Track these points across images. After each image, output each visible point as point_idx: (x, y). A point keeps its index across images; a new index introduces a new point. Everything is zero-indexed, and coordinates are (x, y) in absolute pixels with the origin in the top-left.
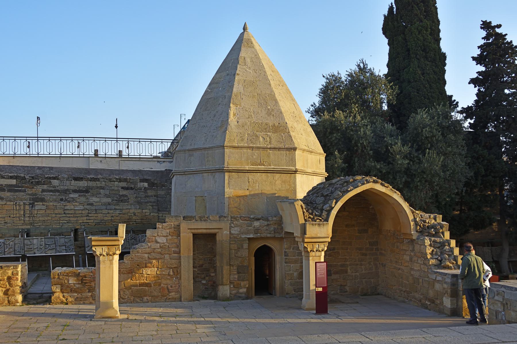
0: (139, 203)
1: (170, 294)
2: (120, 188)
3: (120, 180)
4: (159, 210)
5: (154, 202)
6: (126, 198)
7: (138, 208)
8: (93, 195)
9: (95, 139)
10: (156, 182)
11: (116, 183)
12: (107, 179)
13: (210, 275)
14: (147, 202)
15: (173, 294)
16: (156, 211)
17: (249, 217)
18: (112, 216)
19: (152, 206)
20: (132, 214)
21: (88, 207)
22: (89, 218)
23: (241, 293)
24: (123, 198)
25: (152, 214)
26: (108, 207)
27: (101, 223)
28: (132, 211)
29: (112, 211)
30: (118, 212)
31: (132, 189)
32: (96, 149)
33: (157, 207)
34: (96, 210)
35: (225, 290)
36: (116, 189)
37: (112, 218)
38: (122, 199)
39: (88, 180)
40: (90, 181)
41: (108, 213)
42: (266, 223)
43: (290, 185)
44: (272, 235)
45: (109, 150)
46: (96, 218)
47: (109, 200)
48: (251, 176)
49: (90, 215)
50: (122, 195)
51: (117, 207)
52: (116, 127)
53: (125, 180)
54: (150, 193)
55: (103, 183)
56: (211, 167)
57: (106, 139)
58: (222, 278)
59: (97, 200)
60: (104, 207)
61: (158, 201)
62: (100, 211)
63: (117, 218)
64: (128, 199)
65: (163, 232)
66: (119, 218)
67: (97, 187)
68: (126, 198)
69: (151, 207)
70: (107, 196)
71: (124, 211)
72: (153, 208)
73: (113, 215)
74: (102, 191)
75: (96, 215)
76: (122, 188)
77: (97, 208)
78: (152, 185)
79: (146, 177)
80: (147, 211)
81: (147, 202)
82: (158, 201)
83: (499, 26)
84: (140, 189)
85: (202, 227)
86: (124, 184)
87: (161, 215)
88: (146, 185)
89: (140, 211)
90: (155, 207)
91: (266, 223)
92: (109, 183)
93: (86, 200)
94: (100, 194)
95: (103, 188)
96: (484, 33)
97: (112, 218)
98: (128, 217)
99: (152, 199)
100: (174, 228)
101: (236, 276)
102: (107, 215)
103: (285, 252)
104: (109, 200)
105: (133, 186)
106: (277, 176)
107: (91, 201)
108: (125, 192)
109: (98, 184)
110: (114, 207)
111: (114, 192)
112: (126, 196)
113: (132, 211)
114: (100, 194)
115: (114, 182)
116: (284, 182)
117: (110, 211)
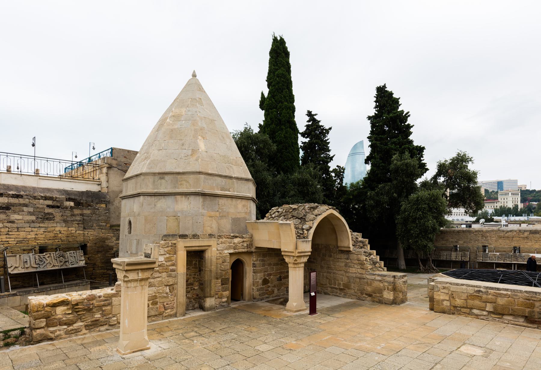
0: (65, 221)
1: (166, 312)
2: (45, 206)
3: (46, 198)
4: (84, 228)
5: (80, 221)
6: (51, 216)
7: (64, 226)
8: (15, 212)
9: (8, 155)
10: (82, 202)
11: (41, 201)
12: (31, 196)
13: (194, 289)
14: (73, 221)
15: (169, 311)
16: (82, 229)
17: (230, 235)
18: (37, 234)
19: (78, 224)
20: (58, 232)
21: (9, 225)
22: (9, 236)
23: (224, 302)
24: (48, 216)
25: (78, 232)
26: (32, 225)
27: (23, 242)
28: (57, 229)
29: (36, 229)
30: (42, 230)
31: (58, 207)
32: (9, 165)
33: (82, 225)
34: (18, 228)
35: (209, 302)
36: (41, 206)
37: (36, 236)
38: (47, 217)
39: (8, 196)
40: (12, 197)
41: (32, 231)
42: (242, 240)
43: (247, 209)
44: (245, 250)
45: (28, 168)
46: (18, 236)
47: (33, 218)
48: (222, 201)
49: (10, 233)
50: (48, 214)
51: (42, 225)
52: (33, 145)
53: (51, 198)
54: (77, 212)
55: (27, 200)
56: (185, 190)
57: (21, 156)
58: (210, 291)
59: (20, 217)
60: (28, 225)
61: (84, 219)
62: (23, 229)
63: (41, 236)
64: (54, 217)
65: (161, 251)
66: (43, 236)
67: (20, 205)
68: (51, 216)
69: (77, 226)
70: (30, 214)
71: (49, 229)
72: (79, 227)
73: (37, 233)
74: (25, 209)
75: (17, 233)
76: (48, 206)
77: (19, 226)
78: (78, 204)
79: (73, 197)
80: (73, 229)
81: (73, 221)
82: (84, 219)
83: (316, 115)
84: (66, 208)
85: (195, 244)
86: (50, 203)
87: (87, 233)
88: (72, 204)
89: (66, 229)
90: (80, 225)
91: (242, 240)
92: (34, 200)
93: (6, 218)
94: (23, 211)
95: (26, 205)
96: (308, 118)
97: (36, 236)
98: (54, 235)
99: (78, 218)
100: (171, 246)
101: (220, 288)
102: (31, 233)
103: (253, 264)
104: (33, 218)
105: (59, 205)
106: (240, 201)
107: (12, 218)
108: (48, 210)
109: (21, 201)
110: (38, 225)
111: (38, 210)
112: (52, 214)
113: (57, 229)
114: (23, 211)
115: (39, 199)
116: (244, 206)
117: (33, 229)
